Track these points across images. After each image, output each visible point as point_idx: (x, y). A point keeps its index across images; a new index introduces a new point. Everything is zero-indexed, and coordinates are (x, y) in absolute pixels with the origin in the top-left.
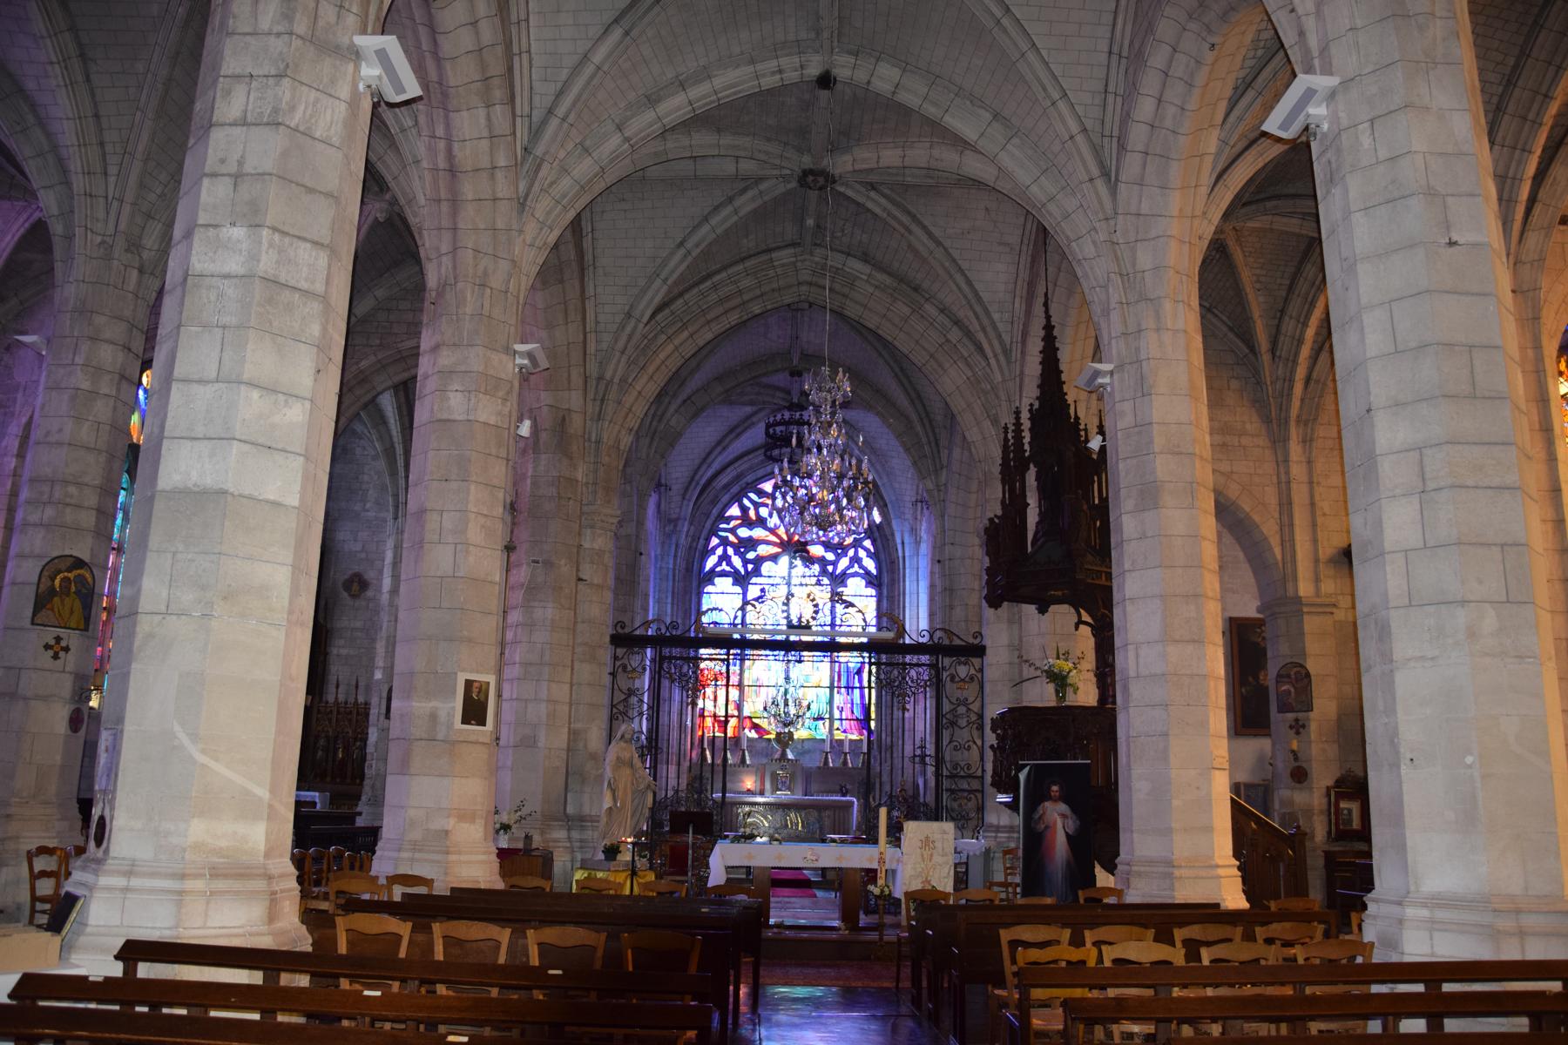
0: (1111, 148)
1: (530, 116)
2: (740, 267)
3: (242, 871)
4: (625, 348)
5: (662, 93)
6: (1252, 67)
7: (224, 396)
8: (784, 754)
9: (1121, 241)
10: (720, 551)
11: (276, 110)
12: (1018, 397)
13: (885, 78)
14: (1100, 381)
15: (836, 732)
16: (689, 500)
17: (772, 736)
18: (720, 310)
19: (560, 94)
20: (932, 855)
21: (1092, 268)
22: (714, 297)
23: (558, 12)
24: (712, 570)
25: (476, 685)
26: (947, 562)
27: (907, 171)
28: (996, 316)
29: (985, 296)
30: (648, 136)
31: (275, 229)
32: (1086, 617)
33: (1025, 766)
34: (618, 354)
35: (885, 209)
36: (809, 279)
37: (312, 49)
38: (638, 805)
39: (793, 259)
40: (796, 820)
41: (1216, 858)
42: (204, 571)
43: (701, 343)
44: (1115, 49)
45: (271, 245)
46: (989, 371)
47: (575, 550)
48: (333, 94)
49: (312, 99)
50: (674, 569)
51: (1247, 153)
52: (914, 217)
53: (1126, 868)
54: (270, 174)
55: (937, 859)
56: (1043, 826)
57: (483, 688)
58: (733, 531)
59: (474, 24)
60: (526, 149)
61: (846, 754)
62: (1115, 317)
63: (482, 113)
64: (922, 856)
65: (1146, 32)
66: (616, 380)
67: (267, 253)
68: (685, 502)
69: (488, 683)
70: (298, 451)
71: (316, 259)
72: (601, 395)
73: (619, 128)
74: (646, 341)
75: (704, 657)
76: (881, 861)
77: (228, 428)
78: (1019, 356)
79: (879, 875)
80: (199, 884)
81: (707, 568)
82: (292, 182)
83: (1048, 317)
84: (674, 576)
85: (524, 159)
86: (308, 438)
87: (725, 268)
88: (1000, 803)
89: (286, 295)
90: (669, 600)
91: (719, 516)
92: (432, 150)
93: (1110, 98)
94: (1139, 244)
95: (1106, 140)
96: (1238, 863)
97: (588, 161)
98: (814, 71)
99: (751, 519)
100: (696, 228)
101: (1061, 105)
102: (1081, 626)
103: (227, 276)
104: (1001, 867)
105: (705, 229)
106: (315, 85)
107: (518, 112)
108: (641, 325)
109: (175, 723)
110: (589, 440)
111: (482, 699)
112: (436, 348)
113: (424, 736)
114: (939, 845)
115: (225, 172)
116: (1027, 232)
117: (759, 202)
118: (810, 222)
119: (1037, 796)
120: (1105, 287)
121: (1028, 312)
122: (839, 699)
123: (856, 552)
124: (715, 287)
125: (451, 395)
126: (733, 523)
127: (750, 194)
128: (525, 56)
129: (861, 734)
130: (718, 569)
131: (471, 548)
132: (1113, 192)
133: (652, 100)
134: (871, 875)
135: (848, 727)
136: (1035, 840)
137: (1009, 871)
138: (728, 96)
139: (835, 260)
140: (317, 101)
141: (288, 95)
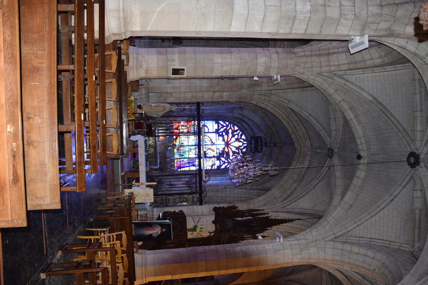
0: (344, 239)
1: (345, 75)
2: (305, 131)
3: (126, 25)
4: (280, 101)
5: (354, 111)
6: (369, 278)
7: (261, 8)
8: (170, 146)
9: (317, 243)
10: (225, 125)
11: (345, 15)
12: (272, 211)
13: (361, 173)
14: (278, 239)
15: (177, 160)
16: (238, 116)
17: (174, 143)
18: (292, 126)
19: (352, 83)
20: (144, 196)
21: (309, 235)
22: (296, 124)
23: (376, 81)
24: (219, 123)
25: (183, 72)
26: (225, 190)
27: (334, 178)
28: (294, 204)
29: (300, 201)
30: (341, 108)
31: (310, 18)
32: (212, 234)
33: (170, 221)
34: (278, 99)
35: (323, 172)
36: (302, 150)
37: (363, 23)
38: (153, 113)
39: (308, 146)
40: (152, 150)
41: (148, 278)
42: (210, 7)
43: (283, 121)
44: (372, 240)
45: (305, 17)
46: (279, 202)
47: (223, 91)
48: (351, 30)
49: (348, 24)
50: (219, 113)
51: (344, 276)
52: (321, 180)
53: (144, 253)
54: (326, 15)
55: (143, 198)
56: (154, 227)
57: (182, 74)
58: (230, 128)
59: (372, 59)
60: (336, 74)
61: (171, 163)
62: (296, 242)
63: (346, 62)
64: (144, 194)
65: (378, 250)
66: (271, 99)
67: (303, 16)
68: (238, 115)
69: (184, 75)
70: (246, 30)
71: (302, 30)
72: (266, 95)
73: (343, 100)
74: (282, 106)
75: (195, 122)
76: (142, 184)
77: (252, 10)
78: (284, 211)
79: (138, 183)
80: (122, 14)
81: (220, 122)
82: (324, 21)
83: (295, 220)
84: (217, 113)
85: (333, 74)
86: (250, 32)
87: (304, 127)
88: (160, 214)
89: (291, 23)
90: (210, 112)
91: (234, 124)
92: (334, 48)
93: (358, 239)
94: (316, 248)
95: (346, 238)
96: (147, 283)
97: (333, 92)
98: (362, 154)
99: (234, 133)
100: (315, 119)
101: (355, 225)
102: (209, 234)
103: (295, 5)
104: (142, 214)
105: (315, 122)
106: (353, 25)
107: (346, 72)
108: (287, 105)
109: (166, 3)
110: (254, 92)
111: (180, 73)
112: (277, 53)
113: (168, 58)
114: (147, 198)
115: (326, 2)
116: (318, 212)
117: (323, 137)
118: (318, 151)
119: (162, 225)
120: (304, 239)
121: (296, 213)
122: (186, 160)
123: (226, 163)
124: (299, 124)
125: (264, 58)
126: (233, 128)
127: (326, 134)
128: (363, 72)
129: (176, 167)
130: (220, 125)
131: (221, 67)
132: (331, 240)
133: (351, 108)
134: (138, 180)
135: (178, 163)
136: (150, 225)
137: (142, 216)
138: (354, 130)
139: (308, 158)
140: (348, 26)
141: (349, 18)
